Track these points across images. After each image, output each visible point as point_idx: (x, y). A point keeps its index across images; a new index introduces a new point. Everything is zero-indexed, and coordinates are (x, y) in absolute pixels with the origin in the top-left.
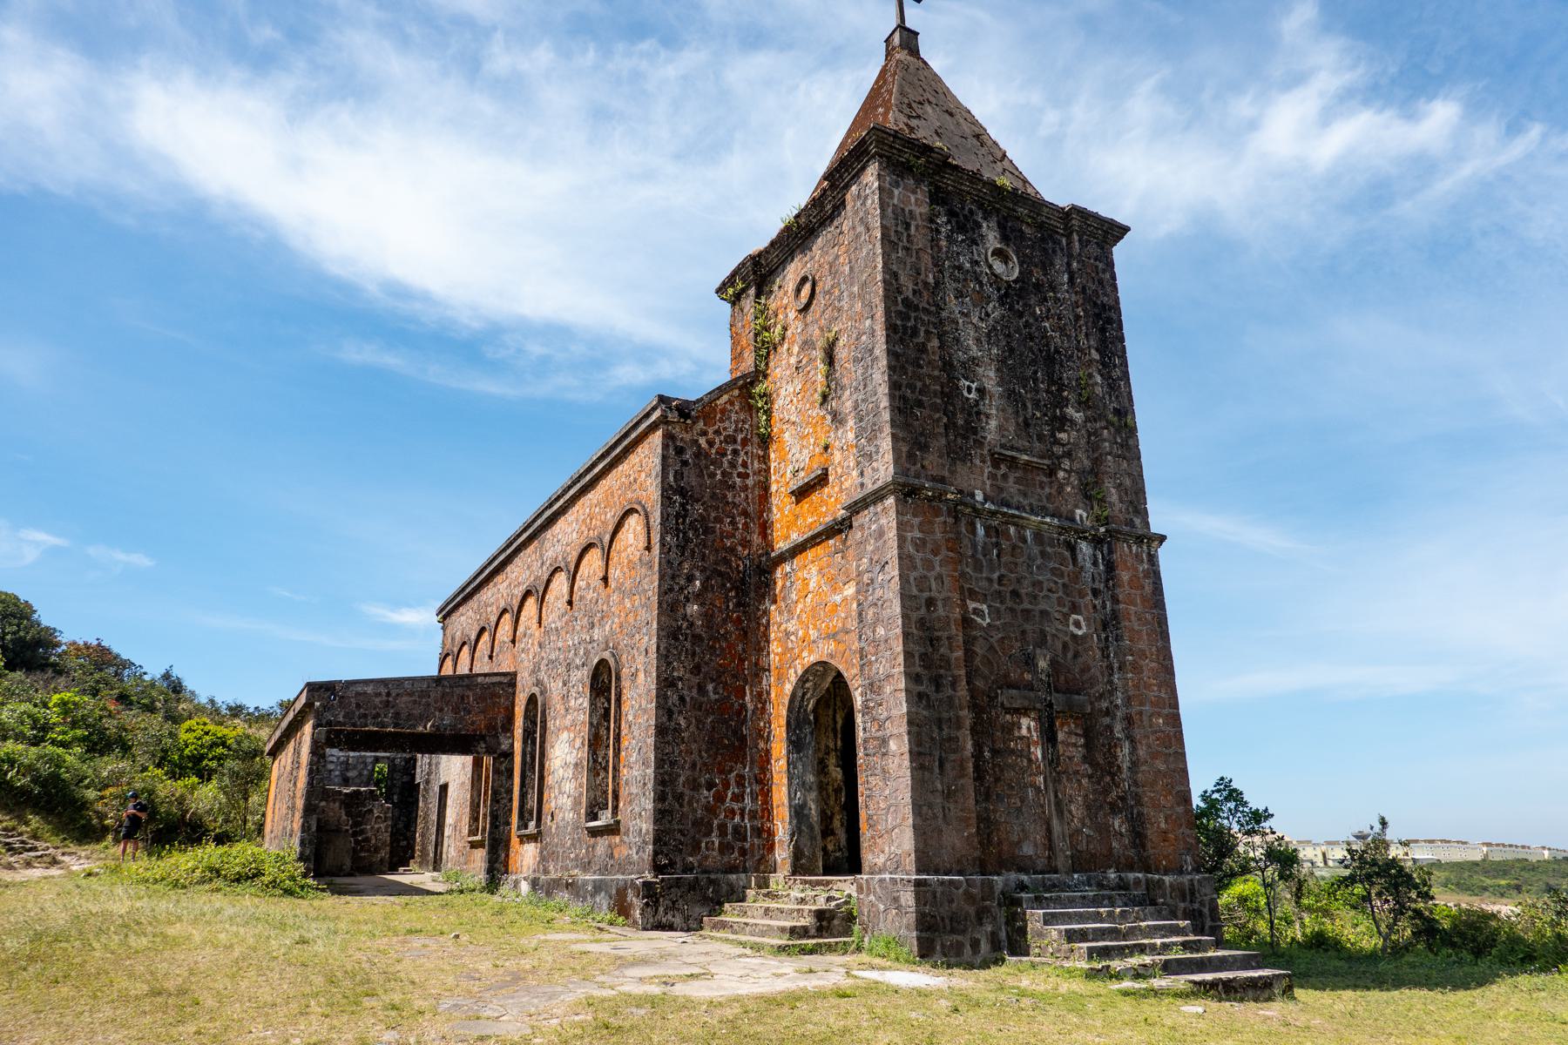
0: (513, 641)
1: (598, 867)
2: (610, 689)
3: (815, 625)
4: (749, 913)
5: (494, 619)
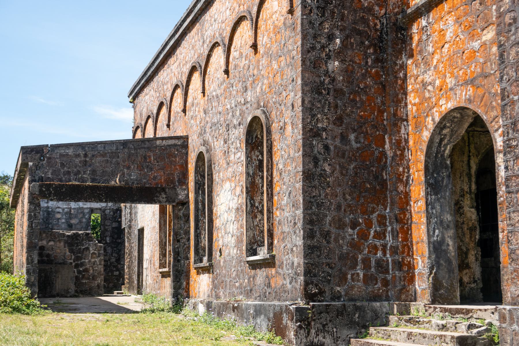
0: (184, 111)
1: (258, 294)
2: (262, 143)
3: (452, 74)
4: (392, 337)
5: (169, 95)
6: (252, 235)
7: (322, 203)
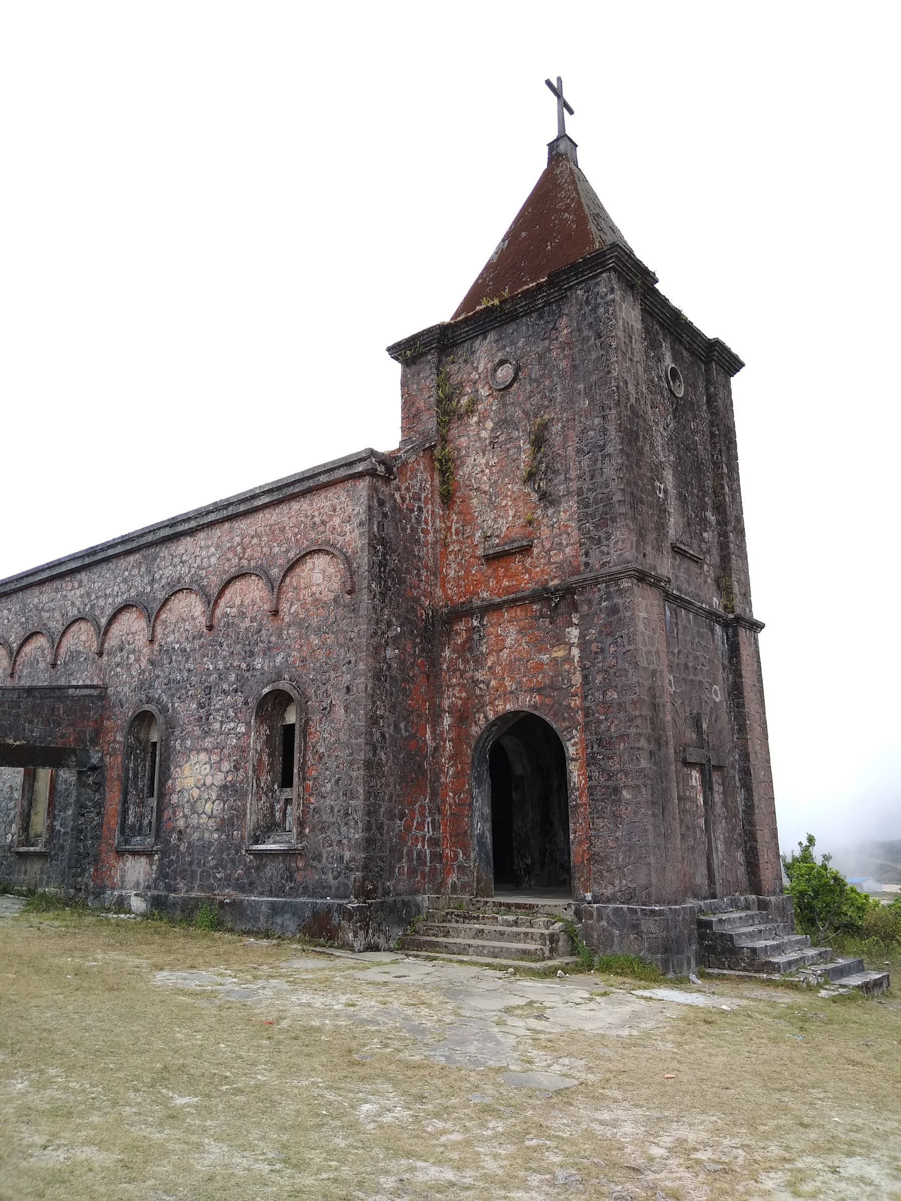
6: (256, 820)
7: (378, 793)
